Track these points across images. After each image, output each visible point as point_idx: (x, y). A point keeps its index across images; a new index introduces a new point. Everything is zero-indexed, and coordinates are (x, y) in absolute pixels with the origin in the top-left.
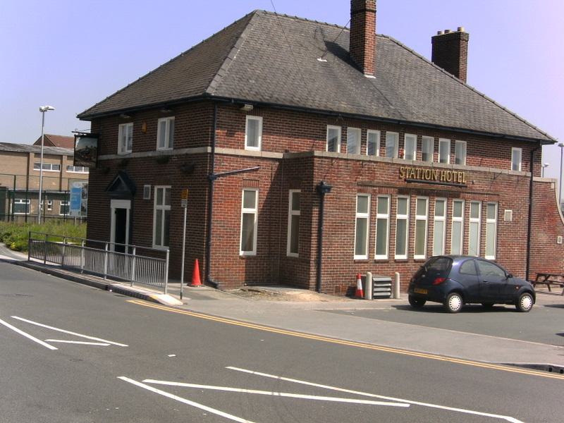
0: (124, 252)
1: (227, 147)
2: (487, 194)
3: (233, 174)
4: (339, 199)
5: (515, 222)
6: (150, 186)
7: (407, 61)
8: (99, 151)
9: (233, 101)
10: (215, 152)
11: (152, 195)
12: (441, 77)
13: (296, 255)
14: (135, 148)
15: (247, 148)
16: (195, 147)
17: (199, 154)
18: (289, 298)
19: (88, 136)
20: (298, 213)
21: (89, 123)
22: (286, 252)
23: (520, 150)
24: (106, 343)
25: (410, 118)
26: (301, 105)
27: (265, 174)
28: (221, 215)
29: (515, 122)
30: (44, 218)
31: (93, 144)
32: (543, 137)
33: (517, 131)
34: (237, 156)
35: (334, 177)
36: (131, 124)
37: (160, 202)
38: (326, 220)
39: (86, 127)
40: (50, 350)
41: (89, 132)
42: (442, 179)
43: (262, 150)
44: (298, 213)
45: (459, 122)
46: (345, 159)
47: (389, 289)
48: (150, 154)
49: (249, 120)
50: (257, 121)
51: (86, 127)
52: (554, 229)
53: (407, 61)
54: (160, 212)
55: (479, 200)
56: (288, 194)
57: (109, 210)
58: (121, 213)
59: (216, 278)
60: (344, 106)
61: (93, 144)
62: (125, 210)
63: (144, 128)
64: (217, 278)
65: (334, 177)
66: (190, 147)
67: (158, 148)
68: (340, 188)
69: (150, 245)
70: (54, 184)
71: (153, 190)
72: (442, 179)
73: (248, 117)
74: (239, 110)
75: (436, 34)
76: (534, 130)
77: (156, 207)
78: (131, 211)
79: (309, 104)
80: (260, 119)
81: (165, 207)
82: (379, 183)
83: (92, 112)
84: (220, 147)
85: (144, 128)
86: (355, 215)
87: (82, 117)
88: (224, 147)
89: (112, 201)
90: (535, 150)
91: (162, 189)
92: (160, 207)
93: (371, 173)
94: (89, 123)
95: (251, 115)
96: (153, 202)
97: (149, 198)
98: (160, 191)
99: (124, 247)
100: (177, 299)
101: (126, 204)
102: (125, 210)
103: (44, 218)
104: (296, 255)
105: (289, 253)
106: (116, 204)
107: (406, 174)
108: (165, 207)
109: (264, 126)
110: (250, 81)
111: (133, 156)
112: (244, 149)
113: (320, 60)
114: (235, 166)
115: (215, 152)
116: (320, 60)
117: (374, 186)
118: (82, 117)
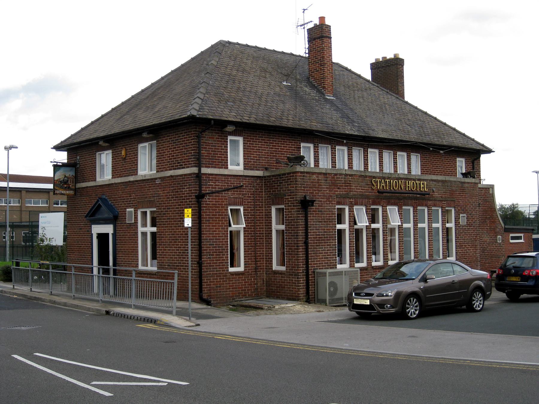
0: (132, 276)
1: (212, 167)
2: (445, 201)
3: (218, 192)
4: (321, 211)
5: (469, 225)
6: (133, 209)
7: (357, 84)
8: (77, 179)
9: (213, 122)
10: (202, 172)
11: (136, 218)
12: (387, 98)
13: (283, 268)
14: (115, 173)
15: (230, 167)
16: (179, 168)
17: (185, 175)
18: (283, 311)
19: (64, 165)
20: (282, 227)
21: (65, 154)
22: (272, 266)
23: (463, 160)
24: (164, 382)
25: (373, 134)
26: (277, 124)
27: (247, 192)
28: (210, 234)
29: (457, 135)
30: (13, 247)
31: (70, 173)
32: (481, 147)
33: (459, 142)
34: (222, 175)
35: (316, 190)
36: (110, 152)
37: (144, 225)
38: (311, 232)
39: (62, 157)
40: (106, 397)
41: (66, 161)
42: (407, 189)
43: (245, 169)
44: (282, 227)
45: (413, 137)
46: (324, 174)
47: (155, 284)
48: (131, 178)
49: (230, 140)
50: (238, 141)
51: (62, 157)
52: (494, 229)
53: (357, 84)
54: (144, 234)
55: (439, 207)
56: (271, 210)
57: (137, 233)
58: (103, 238)
59: (209, 296)
60: (315, 126)
61: (70, 173)
62: (108, 234)
63: (123, 153)
64: (210, 295)
65: (316, 190)
66: (175, 169)
67: (98, 179)
68: (321, 201)
69: (137, 266)
70: (15, 216)
71: (136, 212)
72: (407, 189)
73: (230, 138)
74: (221, 131)
75: (374, 61)
76: (472, 142)
77: (141, 229)
78: (114, 235)
79: (285, 123)
80: (240, 139)
81: (150, 229)
82: (354, 195)
83: (71, 141)
84: (206, 167)
85: (123, 153)
86: (336, 227)
87: (58, 148)
88: (209, 167)
89: (93, 226)
90: (475, 159)
91: (146, 212)
92: (144, 229)
93: (347, 186)
94: (65, 154)
95: (232, 135)
96: (137, 225)
97: (133, 222)
98: (144, 214)
99: (108, 269)
100: (187, 320)
101: (108, 229)
102: (108, 234)
103: (13, 247)
104: (283, 268)
105: (275, 267)
106: (97, 229)
107: (377, 185)
108: (150, 229)
109: (244, 146)
110: (229, 103)
111: (113, 182)
112: (227, 168)
113: (285, 83)
114: (220, 185)
115: (202, 172)
116: (285, 83)
117: (350, 198)
118: (58, 148)
